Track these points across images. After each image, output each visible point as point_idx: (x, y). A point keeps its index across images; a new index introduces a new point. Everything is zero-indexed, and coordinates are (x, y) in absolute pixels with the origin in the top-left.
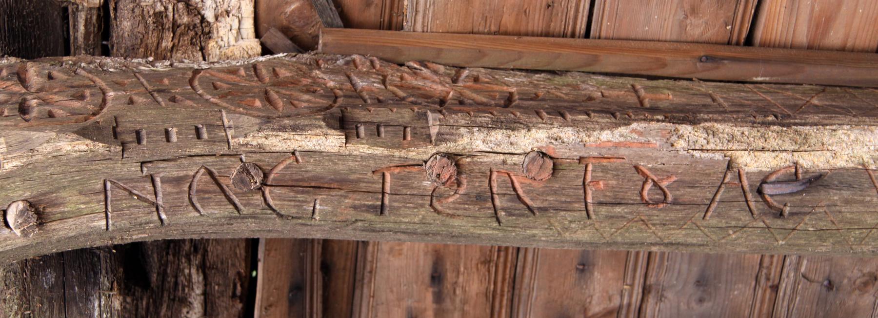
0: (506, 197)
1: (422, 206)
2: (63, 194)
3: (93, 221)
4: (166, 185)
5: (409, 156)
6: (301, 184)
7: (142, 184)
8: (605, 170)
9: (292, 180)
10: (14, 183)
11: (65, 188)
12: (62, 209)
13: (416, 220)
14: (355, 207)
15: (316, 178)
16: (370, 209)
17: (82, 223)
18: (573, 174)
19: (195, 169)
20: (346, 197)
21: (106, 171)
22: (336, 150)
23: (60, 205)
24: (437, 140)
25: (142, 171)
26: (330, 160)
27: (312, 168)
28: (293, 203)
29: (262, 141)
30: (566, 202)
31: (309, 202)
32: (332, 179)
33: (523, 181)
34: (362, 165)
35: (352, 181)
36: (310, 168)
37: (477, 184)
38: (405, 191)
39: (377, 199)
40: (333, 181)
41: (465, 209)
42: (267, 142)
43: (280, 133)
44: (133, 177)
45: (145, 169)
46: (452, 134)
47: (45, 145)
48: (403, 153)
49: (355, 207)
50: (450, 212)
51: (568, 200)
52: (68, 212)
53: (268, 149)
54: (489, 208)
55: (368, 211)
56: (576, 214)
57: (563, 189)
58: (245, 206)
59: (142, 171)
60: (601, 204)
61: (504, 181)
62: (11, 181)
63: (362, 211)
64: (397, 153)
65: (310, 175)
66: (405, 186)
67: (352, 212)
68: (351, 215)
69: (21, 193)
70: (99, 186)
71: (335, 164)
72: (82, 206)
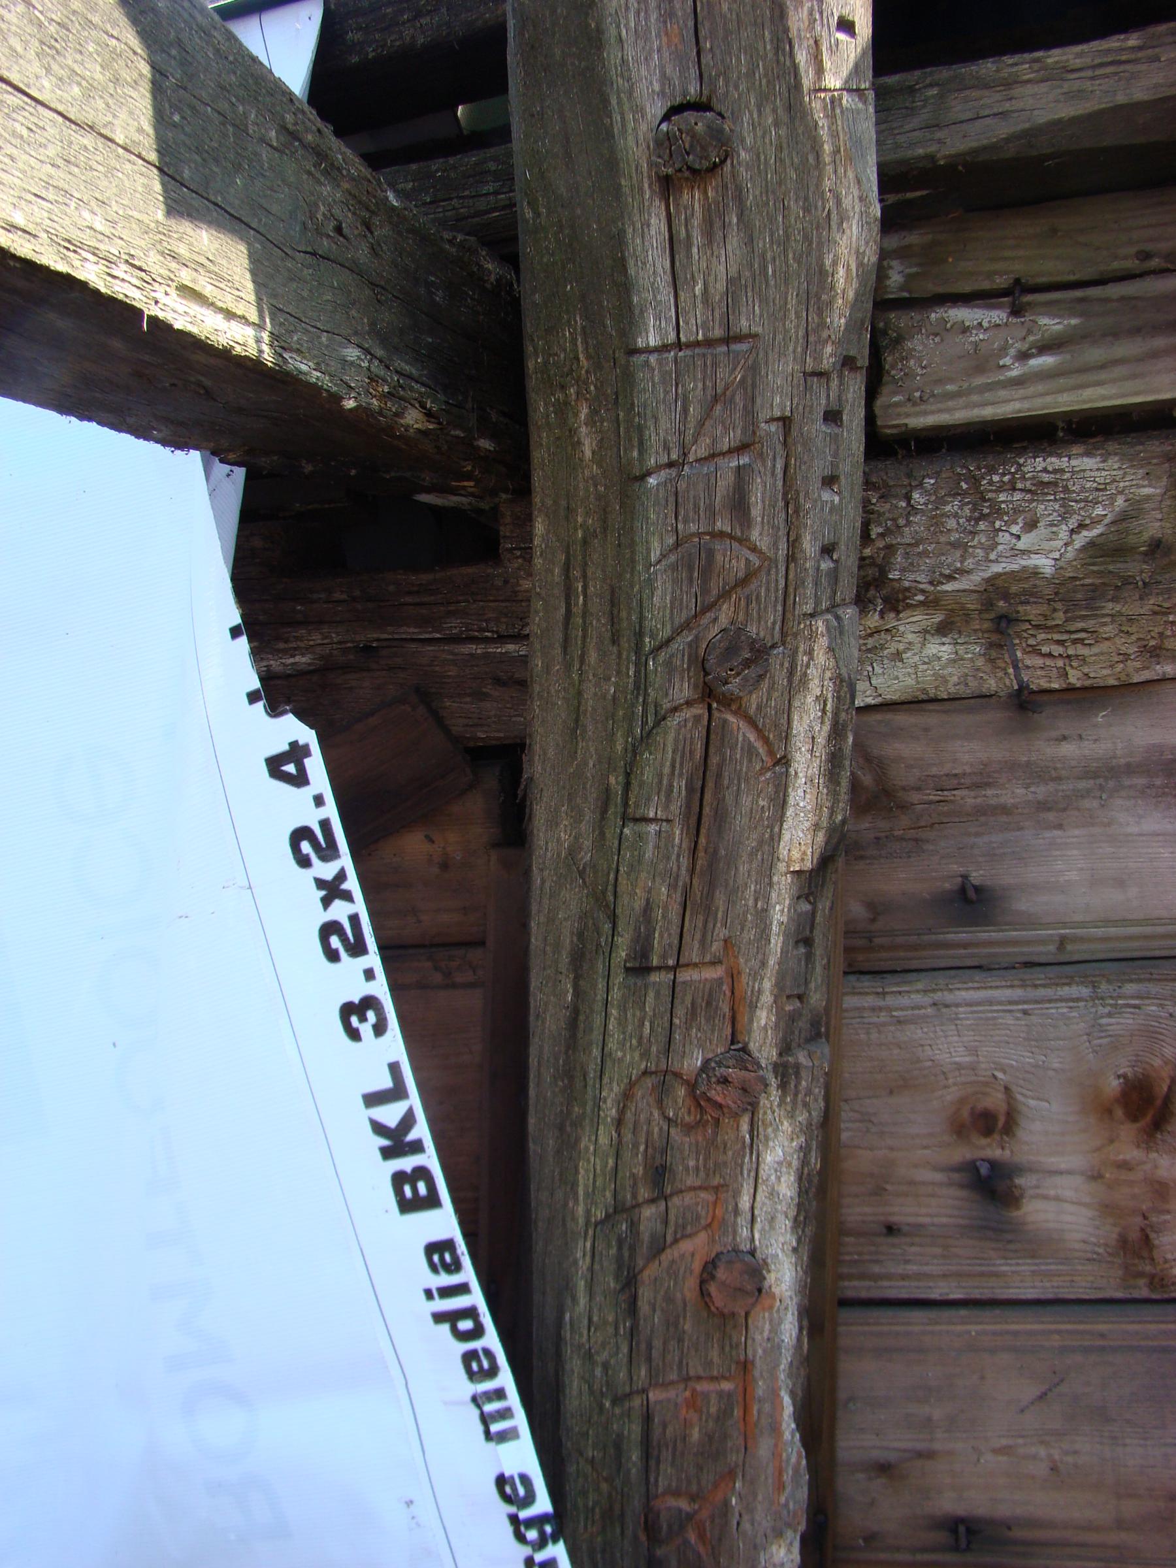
0: (660, 1227)
1: (645, 1055)
2: (734, 241)
3: (658, 318)
4: (731, 478)
5: (758, 1012)
6: (710, 784)
7: (740, 424)
8: (724, 1414)
9: (720, 766)
10: (777, 124)
11: (750, 241)
12: (697, 238)
13: (612, 1045)
14: (648, 909)
15: (721, 817)
16: (642, 949)
17: (655, 291)
18: (714, 1354)
19: (763, 544)
20: (672, 887)
21: (779, 337)
22: (783, 852)
23: (709, 234)
24: (785, 1066)
25: (773, 420)
26: (761, 842)
27: (748, 803)
28: (667, 770)
29: (815, 688)
30: (650, 1347)
31: (666, 808)
32: (716, 852)
33: (697, 1257)
34: (745, 913)
35: (710, 895)
36: (746, 801)
37: (692, 1163)
38: (680, 1011)
39: (664, 957)
40: (714, 856)
41: (636, 1145)
42: (810, 699)
43: (827, 728)
44: (759, 401)
45: (773, 428)
46: (794, 1102)
47: (856, 193)
48: (767, 998)
49: (648, 909)
50: (629, 1115)
51: (655, 1353)
52: (689, 256)
53: (796, 703)
54: (634, 1196)
55: (637, 939)
56: (623, 1375)
57: (680, 1340)
58: (668, 663)
59: (773, 420)
60: (648, 1418)
61: (698, 1217)
62: (784, 117)
63: (637, 929)
64: (767, 985)
65: (729, 799)
66: (693, 1013)
67: (639, 904)
68: (631, 903)
69: (749, 141)
70: (744, 324)
71: (752, 854)
72: (698, 289)
